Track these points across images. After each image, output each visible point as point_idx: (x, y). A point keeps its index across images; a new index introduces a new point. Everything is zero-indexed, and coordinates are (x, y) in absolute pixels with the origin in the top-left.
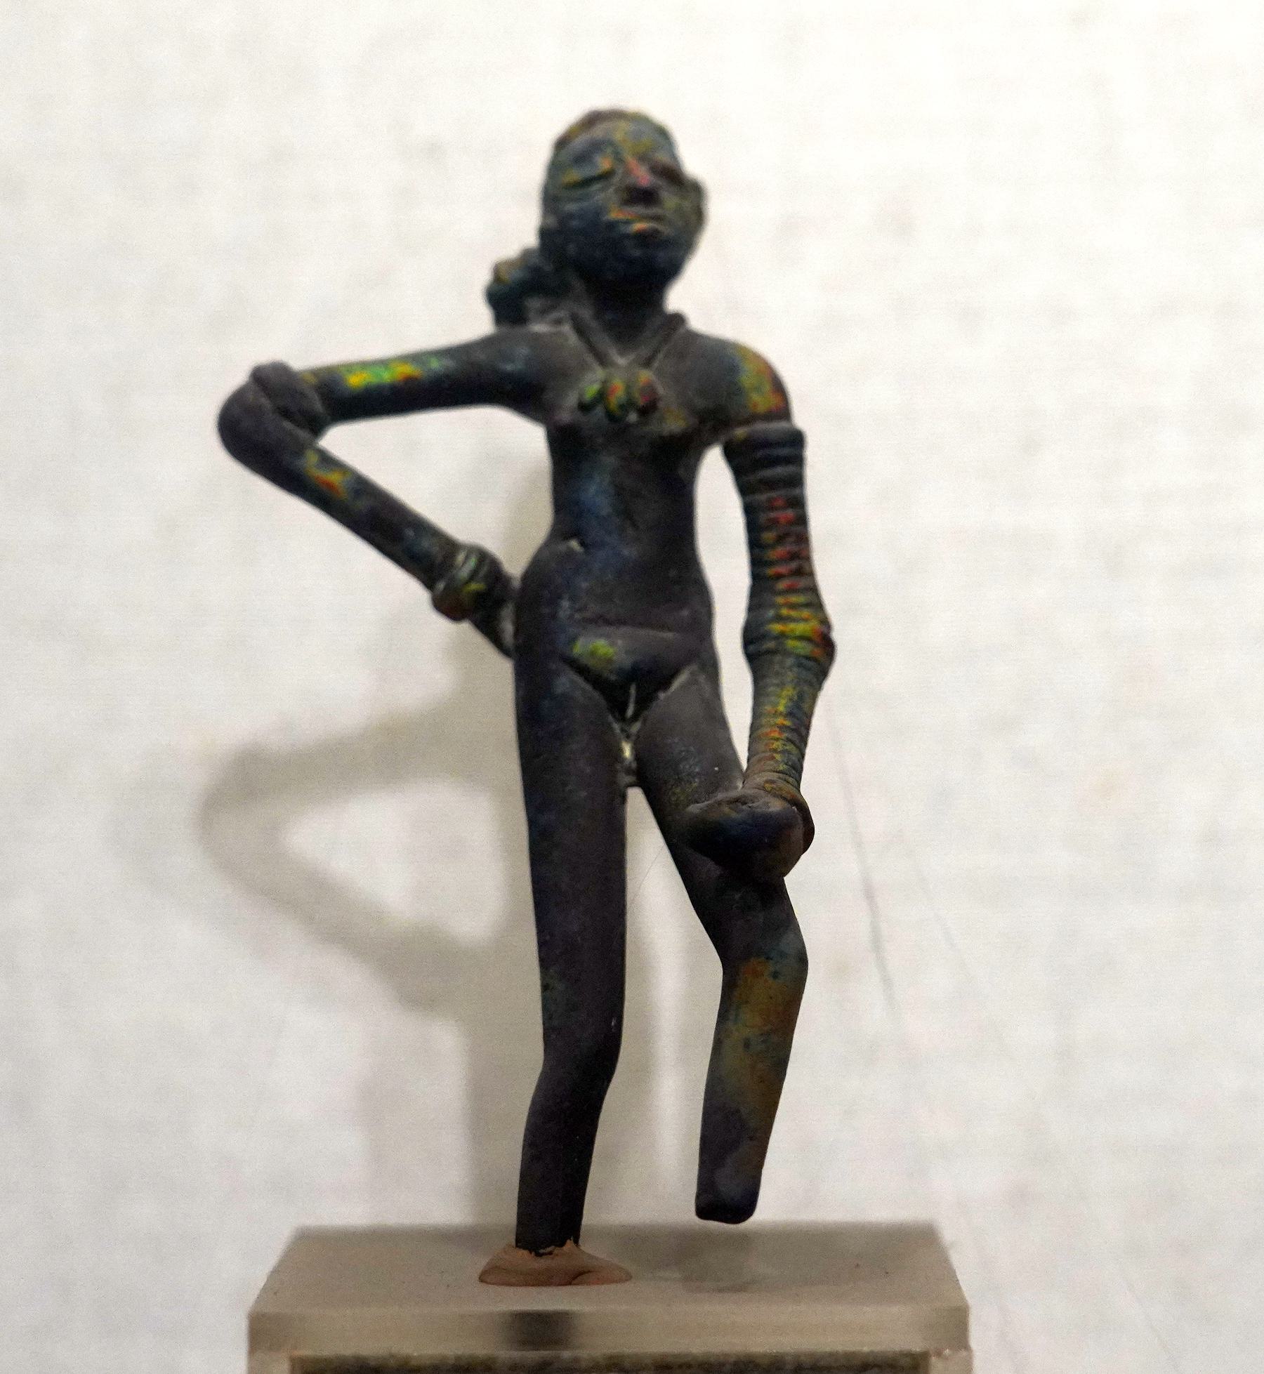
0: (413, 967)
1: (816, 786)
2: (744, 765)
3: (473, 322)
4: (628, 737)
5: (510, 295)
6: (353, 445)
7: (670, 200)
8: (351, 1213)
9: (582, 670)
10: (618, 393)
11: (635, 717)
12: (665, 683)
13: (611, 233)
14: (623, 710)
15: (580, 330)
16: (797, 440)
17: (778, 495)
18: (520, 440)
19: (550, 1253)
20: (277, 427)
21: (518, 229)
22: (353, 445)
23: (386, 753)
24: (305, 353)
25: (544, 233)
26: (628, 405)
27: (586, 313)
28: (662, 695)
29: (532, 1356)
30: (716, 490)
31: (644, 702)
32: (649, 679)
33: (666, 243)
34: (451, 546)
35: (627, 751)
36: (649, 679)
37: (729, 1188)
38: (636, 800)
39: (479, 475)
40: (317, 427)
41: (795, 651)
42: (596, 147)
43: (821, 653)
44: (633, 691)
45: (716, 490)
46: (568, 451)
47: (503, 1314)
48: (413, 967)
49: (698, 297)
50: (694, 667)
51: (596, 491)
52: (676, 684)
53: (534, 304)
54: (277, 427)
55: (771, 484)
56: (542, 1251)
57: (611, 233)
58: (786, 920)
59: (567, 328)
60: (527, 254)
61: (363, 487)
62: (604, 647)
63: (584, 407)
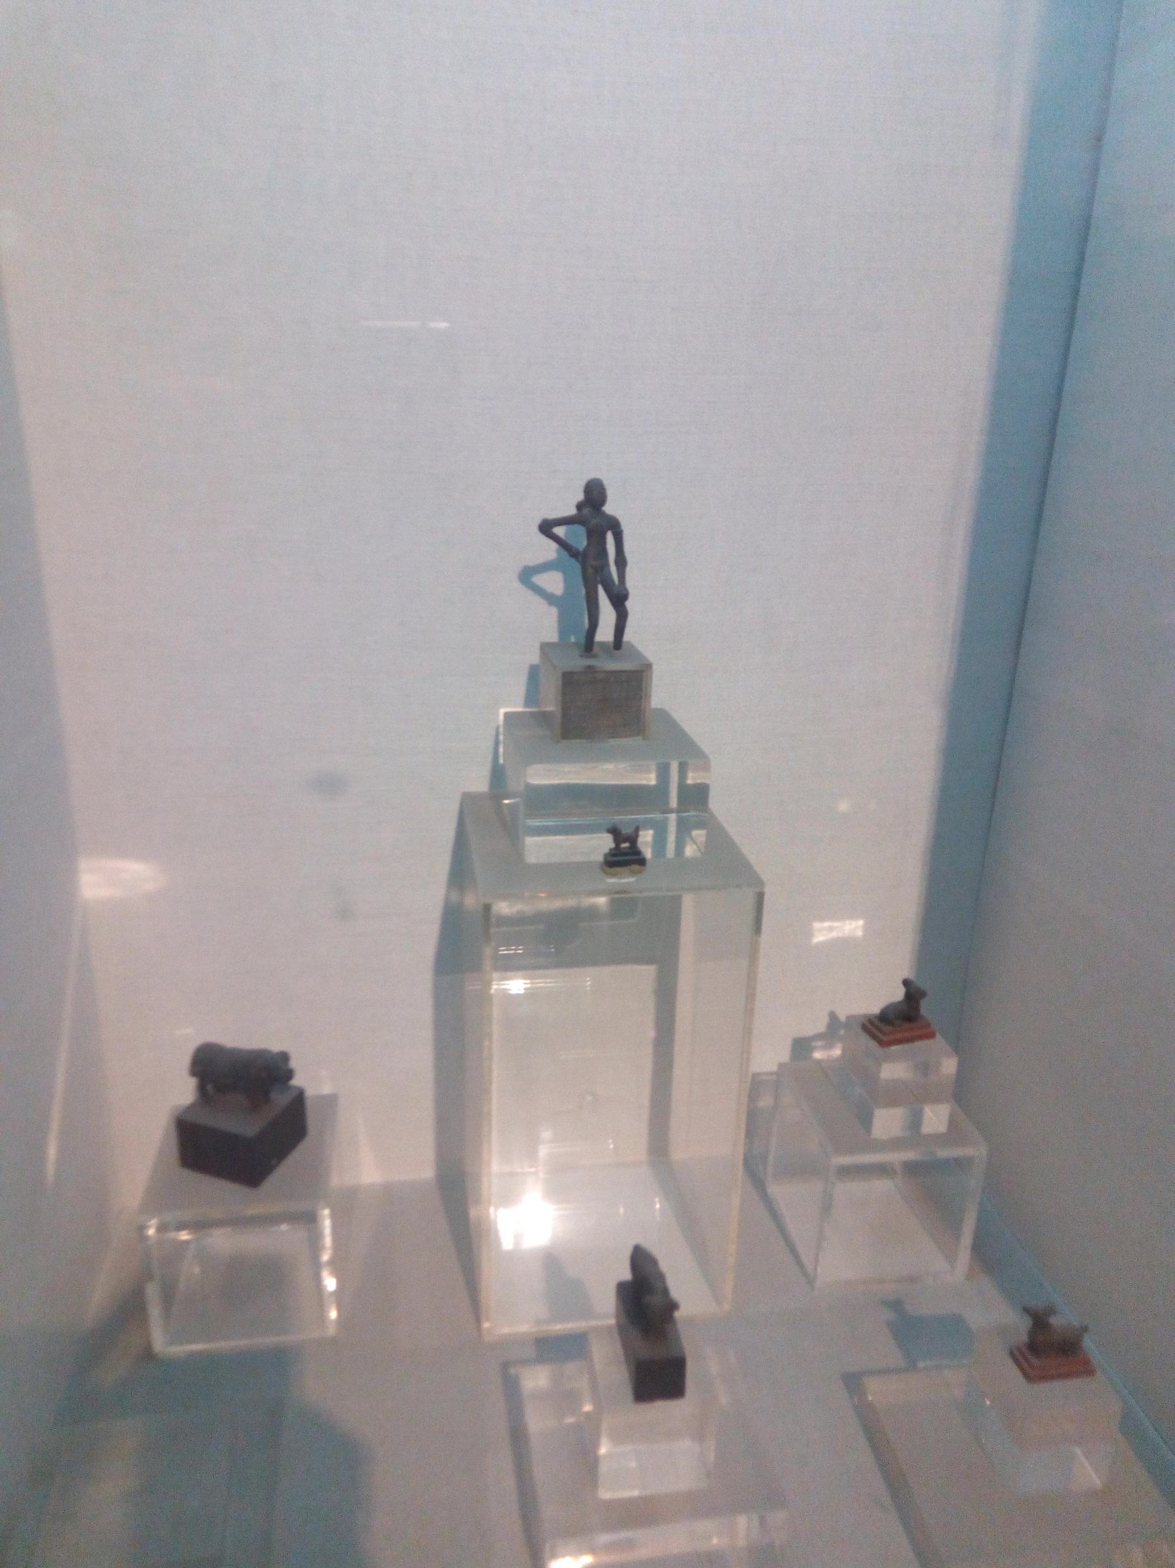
1: (630, 583)
5: (579, 507)
13: (594, 495)
20: (546, 528)
21: (580, 497)
41: (621, 562)
49: (609, 509)
54: (546, 528)
57: (594, 495)
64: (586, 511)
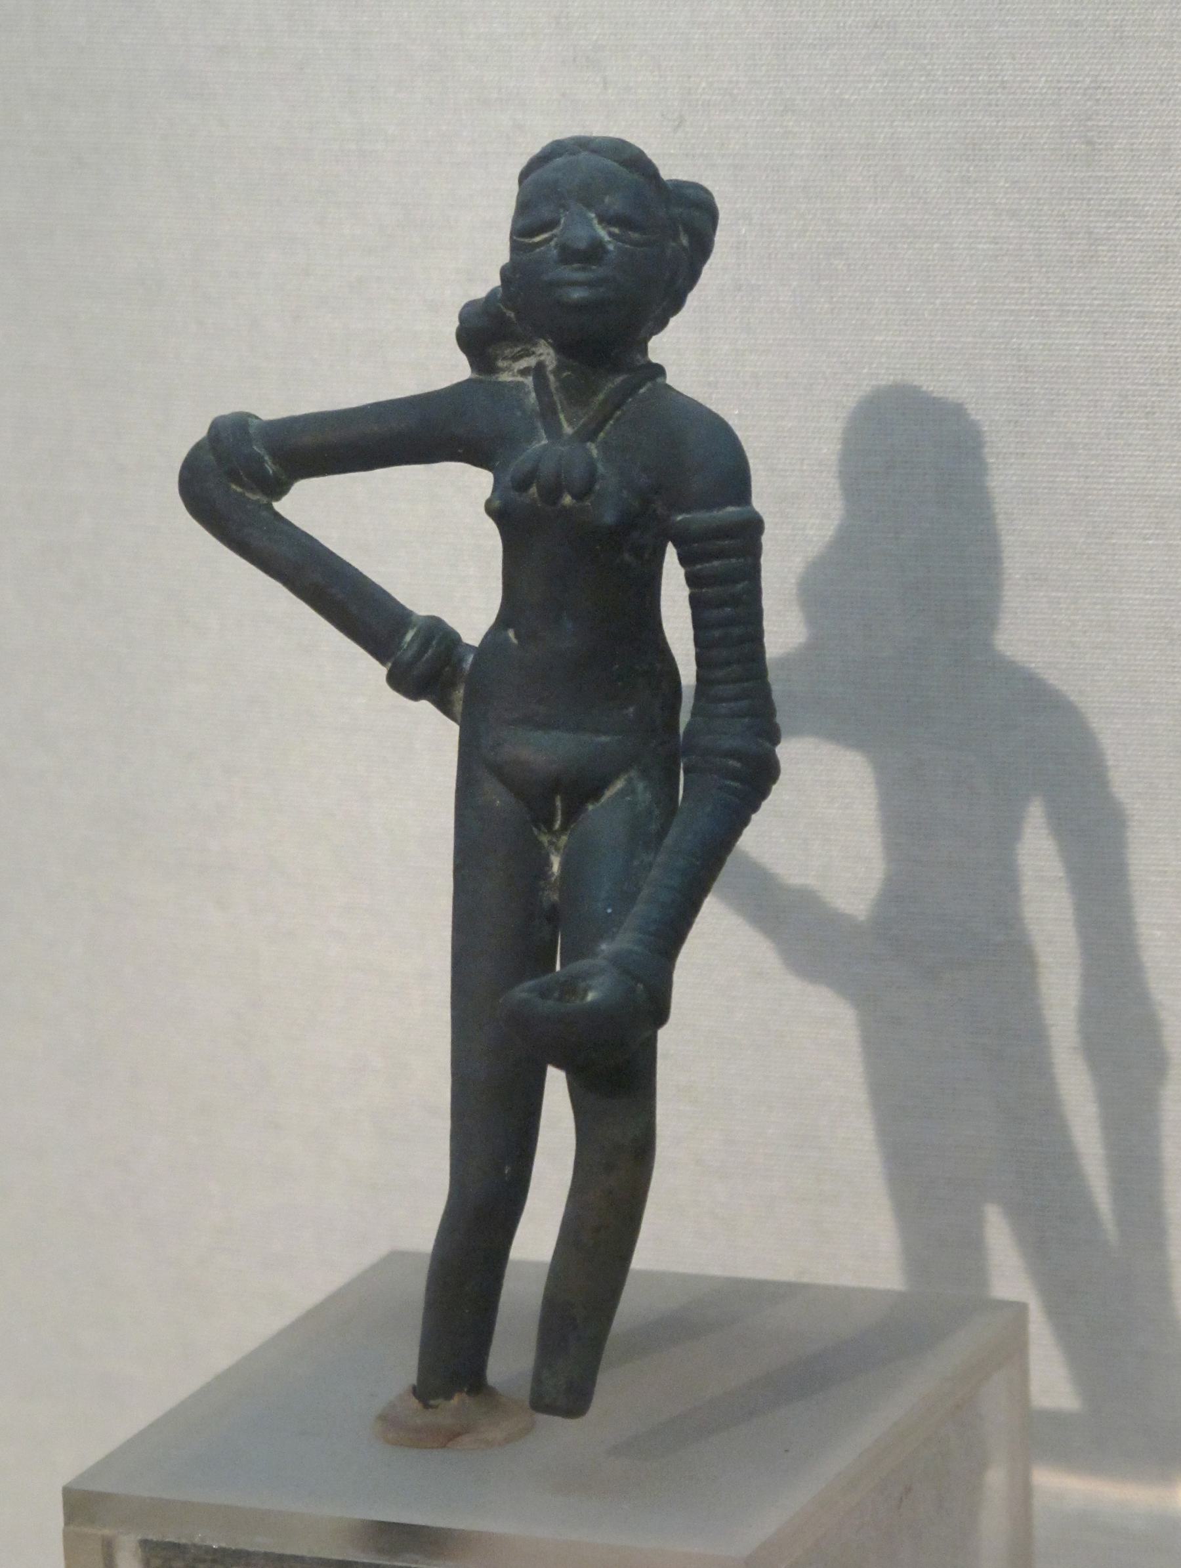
2: (556, 1083)
4: (557, 849)
5: (481, 333)
6: (317, 507)
11: (564, 828)
12: (595, 793)
13: (603, 256)
14: (549, 823)
16: (755, 526)
18: (457, 496)
19: (436, 1407)
20: (239, 482)
21: (479, 261)
22: (317, 507)
24: (274, 403)
28: (590, 807)
30: (1039, 855)
31: (572, 813)
35: (556, 868)
39: (434, 538)
40: (279, 489)
44: (558, 803)
45: (1039, 855)
47: (363, 1521)
49: (689, 352)
50: (633, 773)
52: (609, 793)
54: (239, 482)
56: (432, 1402)
57: (603, 256)
59: (529, 381)
60: (493, 294)
64: (528, 366)
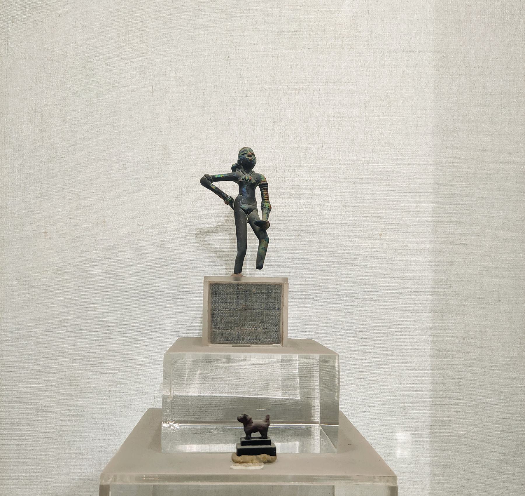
0: (219, 253)
3: (229, 171)
5: (234, 168)
6: (216, 184)
7: (253, 157)
8: (185, 336)
9: (243, 209)
10: (247, 178)
13: (246, 162)
15: (242, 172)
16: (267, 184)
17: (265, 191)
20: (207, 182)
23: (217, 229)
25: (238, 161)
26: (248, 179)
27: (243, 170)
29: (237, 282)
30: (258, 189)
32: (249, 211)
33: (252, 161)
34: (227, 196)
36: (249, 211)
37: (260, 264)
38: (248, 225)
41: (267, 208)
42: (245, 150)
43: (270, 209)
45: (258, 189)
46: (241, 185)
48: (219, 253)
51: (244, 189)
53: (237, 169)
54: (207, 182)
55: (264, 189)
57: (246, 162)
58: (266, 235)
61: (217, 188)
62: (245, 206)
63: (243, 179)
